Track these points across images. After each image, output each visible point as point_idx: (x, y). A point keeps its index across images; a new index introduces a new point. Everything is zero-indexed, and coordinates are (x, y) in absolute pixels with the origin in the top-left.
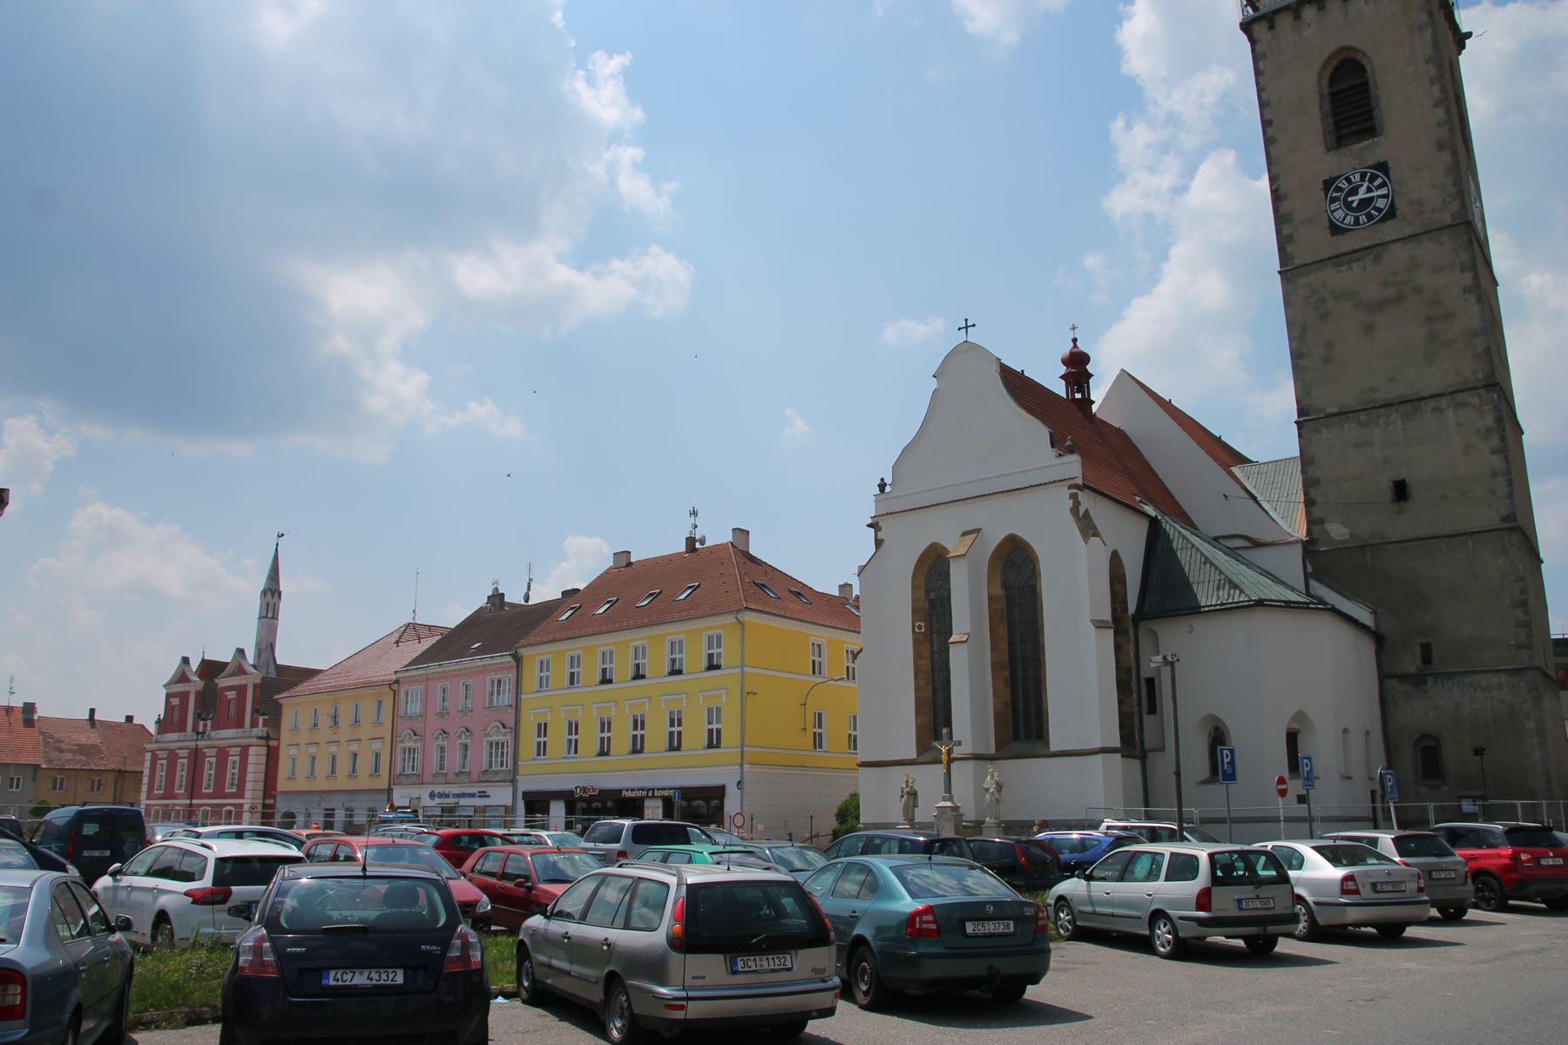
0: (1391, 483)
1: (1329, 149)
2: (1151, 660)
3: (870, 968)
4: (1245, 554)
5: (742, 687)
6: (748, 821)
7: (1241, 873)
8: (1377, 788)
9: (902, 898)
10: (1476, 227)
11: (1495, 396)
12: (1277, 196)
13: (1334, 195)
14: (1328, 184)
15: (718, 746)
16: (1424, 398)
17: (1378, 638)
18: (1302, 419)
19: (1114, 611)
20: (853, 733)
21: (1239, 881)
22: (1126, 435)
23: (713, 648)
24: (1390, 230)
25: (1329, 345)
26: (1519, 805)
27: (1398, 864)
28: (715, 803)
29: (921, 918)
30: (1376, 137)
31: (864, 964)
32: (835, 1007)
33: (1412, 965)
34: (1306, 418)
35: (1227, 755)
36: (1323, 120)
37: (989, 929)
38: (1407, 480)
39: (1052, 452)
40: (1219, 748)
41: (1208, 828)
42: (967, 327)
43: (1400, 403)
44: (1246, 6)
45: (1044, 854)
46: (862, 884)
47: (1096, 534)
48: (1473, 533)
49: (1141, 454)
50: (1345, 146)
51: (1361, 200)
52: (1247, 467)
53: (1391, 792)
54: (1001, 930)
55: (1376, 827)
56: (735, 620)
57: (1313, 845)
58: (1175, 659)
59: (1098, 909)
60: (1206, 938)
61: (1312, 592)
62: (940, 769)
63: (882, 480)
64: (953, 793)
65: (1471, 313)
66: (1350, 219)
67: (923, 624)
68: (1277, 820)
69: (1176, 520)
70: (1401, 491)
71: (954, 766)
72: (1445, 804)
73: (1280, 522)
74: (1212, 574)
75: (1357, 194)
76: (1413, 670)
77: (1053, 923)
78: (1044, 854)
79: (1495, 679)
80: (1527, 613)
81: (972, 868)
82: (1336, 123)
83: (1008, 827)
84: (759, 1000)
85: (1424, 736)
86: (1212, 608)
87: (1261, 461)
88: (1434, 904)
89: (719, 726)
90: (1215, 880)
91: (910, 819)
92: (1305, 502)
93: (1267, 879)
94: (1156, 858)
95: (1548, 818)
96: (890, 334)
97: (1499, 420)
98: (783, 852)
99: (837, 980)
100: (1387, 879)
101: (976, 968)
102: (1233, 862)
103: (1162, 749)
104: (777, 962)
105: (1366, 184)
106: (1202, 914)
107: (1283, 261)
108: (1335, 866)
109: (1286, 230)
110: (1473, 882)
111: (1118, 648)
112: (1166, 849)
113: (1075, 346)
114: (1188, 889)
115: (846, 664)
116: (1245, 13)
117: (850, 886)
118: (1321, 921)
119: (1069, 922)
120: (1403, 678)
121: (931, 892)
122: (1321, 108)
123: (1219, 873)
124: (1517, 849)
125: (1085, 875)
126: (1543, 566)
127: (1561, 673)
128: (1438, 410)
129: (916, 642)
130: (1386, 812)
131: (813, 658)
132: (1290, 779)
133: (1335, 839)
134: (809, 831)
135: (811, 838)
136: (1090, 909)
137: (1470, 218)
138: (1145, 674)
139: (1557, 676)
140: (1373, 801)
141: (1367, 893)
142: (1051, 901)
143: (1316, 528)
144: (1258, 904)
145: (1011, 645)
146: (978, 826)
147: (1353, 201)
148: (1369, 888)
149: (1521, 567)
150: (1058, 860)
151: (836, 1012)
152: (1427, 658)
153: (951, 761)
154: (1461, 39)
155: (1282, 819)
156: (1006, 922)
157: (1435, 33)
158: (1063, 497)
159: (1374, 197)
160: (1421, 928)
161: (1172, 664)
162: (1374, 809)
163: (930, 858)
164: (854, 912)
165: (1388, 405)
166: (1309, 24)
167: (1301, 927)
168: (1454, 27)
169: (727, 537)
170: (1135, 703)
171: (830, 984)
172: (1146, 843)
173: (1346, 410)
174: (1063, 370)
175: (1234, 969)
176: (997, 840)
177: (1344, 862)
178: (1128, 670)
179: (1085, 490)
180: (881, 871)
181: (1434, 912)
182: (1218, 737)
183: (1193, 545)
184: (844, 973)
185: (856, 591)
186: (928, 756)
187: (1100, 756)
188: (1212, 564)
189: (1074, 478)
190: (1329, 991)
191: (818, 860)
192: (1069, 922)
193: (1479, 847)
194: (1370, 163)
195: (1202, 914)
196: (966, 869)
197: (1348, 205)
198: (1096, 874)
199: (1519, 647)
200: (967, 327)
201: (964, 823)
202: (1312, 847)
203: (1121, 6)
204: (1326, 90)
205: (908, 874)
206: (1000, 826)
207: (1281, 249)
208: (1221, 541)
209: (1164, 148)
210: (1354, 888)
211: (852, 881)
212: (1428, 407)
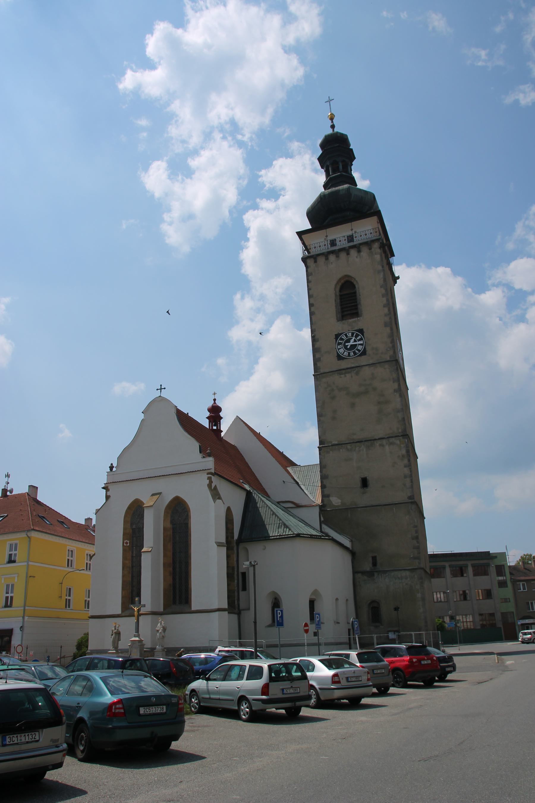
0: (360, 479)
1: (338, 320)
2: (244, 564)
3: (86, 736)
4: (292, 510)
5: (27, 574)
6: (25, 649)
7: (284, 674)
8: (351, 628)
9: (106, 695)
10: (400, 362)
11: (407, 441)
12: (314, 339)
13: (339, 341)
14: (337, 336)
15: (11, 606)
16: (376, 439)
17: (353, 553)
18: (321, 446)
19: (227, 538)
20: (88, 599)
21: (283, 679)
22: (238, 449)
23: (12, 551)
24: (363, 360)
25: (335, 411)
26: (413, 634)
27: (359, 667)
28: (6, 639)
29: (115, 706)
30: (359, 317)
31: (82, 734)
32: (63, 762)
33: (364, 719)
34: (323, 446)
35: (279, 613)
36: (336, 306)
37: (152, 711)
38: (368, 478)
39: (200, 456)
40: (276, 609)
41: (271, 651)
42: (161, 389)
43: (365, 441)
44: (305, 250)
45: (185, 666)
46: (84, 687)
47: (220, 498)
48: (396, 504)
49: (244, 459)
50: (345, 320)
51: (351, 345)
52: (295, 468)
53: (357, 630)
54: (159, 711)
55: (350, 648)
56: (26, 536)
57: (319, 659)
58: (256, 564)
59: (212, 696)
60: (266, 710)
61: (323, 530)
62: (133, 620)
63: (112, 464)
64: (139, 633)
65: (397, 402)
66: (346, 353)
67: (128, 542)
68: (303, 645)
69: (260, 493)
70: (365, 483)
71: (141, 618)
72: (382, 635)
73: (309, 495)
74: (276, 521)
75: (349, 342)
76: (368, 569)
77: (189, 704)
78: (185, 666)
79: (404, 574)
80: (418, 542)
81: (146, 677)
82: (342, 309)
83: (169, 651)
84: (17, 761)
85: (373, 602)
86: (275, 537)
87: (301, 465)
88: (374, 686)
89: (12, 595)
90: (271, 679)
91: (116, 647)
92: (321, 486)
93: (297, 677)
94: (242, 668)
95: (426, 640)
96: (117, 389)
97: (408, 451)
98: (42, 669)
99: (65, 746)
100: (353, 675)
101: (144, 733)
102: (281, 669)
103: (249, 609)
104: (30, 737)
105: (354, 338)
106: (264, 697)
107: (315, 370)
108: (329, 669)
109: (318, 356)
110: (392, 674)
111: (228, 556)
112: (247, 663)
113: (215, 403)
114: (258, 683)
115: (86, 561)
116: (304, 254)
117: (78, 688)
118: (322, 698)
119: (197, 703)
120: (363, 573)
121: (121, 690)
122: (335, 301)
123: (273, 675)
124: (411, 657)
125: (206, 678)
126: (425, 520)
127: (432, 570)
128: (382, 445)
129: (124, 551)
130: (355, 639)
131: (68, 558)
132: (311, 624)
133: (330, 655)
134: (60, 654)
135: (61, 658)
136: (208, 696)
137: (397, 358)
138: (241, 570)
139: (430, 572)
140: (349, 635)
141: (344, 683)
142: (188, 692)
143: (326, 499)
144: (292, 691)
145: (174, 554)
146: (152, 650)
147: (348, 345)
148: (345, 679)
149: (416, 520)
150: (192, 669)
151: (64, 764)
152: (375, 564)
153: (139, 615)
154: (395, 279)
155: (306, 644)
156: (161, 707)
157: (384, 275)
158: (203, 479)
159: (357, 344)
160: (369, 698)
161: (254, 566)
162: (350, 638)
163: (122, 672)
164: (79, 704)
165: (360, 442)
166: (332, 263)
167: (313, 701)
168: (392, 273)
169: (26, 490)
170: (236, 585)
171: (61, 748)
172: (239, 660)
173: (341, 443)
174: (208, 414)
175: (279, 726)
176: (161, 659)
177: (334, 667)
178: (233, 568)
179: (215, 476)
180: (95, 679)
181: (375, 690)
182: (276, 604)
183: (267, 505)
184: (70, 741)
185: (94, 522)
186: (127, 613)
187: (217, 613)
188: (276, 515)
189: (210, 469)
190: (325, 735)
191: (62, 672)
192: (197, 703)
193: (395, 657)
194: (356, 328)
195: (264, 697)
196: (142, 677)
197: (346, 347)
198: (211, 677)
199: (415, 558)
200: (161, 389)
201: (145, 649)
202: (319, 660)
203: (243, 242)
204: (338, 294)
205: (110, 681)
206: (164, 651)
207: (315, 364)
208: (281, 504)
209: (258, 310)
210: (338, 680)
211: (80, 686)
212: (377, 444)
